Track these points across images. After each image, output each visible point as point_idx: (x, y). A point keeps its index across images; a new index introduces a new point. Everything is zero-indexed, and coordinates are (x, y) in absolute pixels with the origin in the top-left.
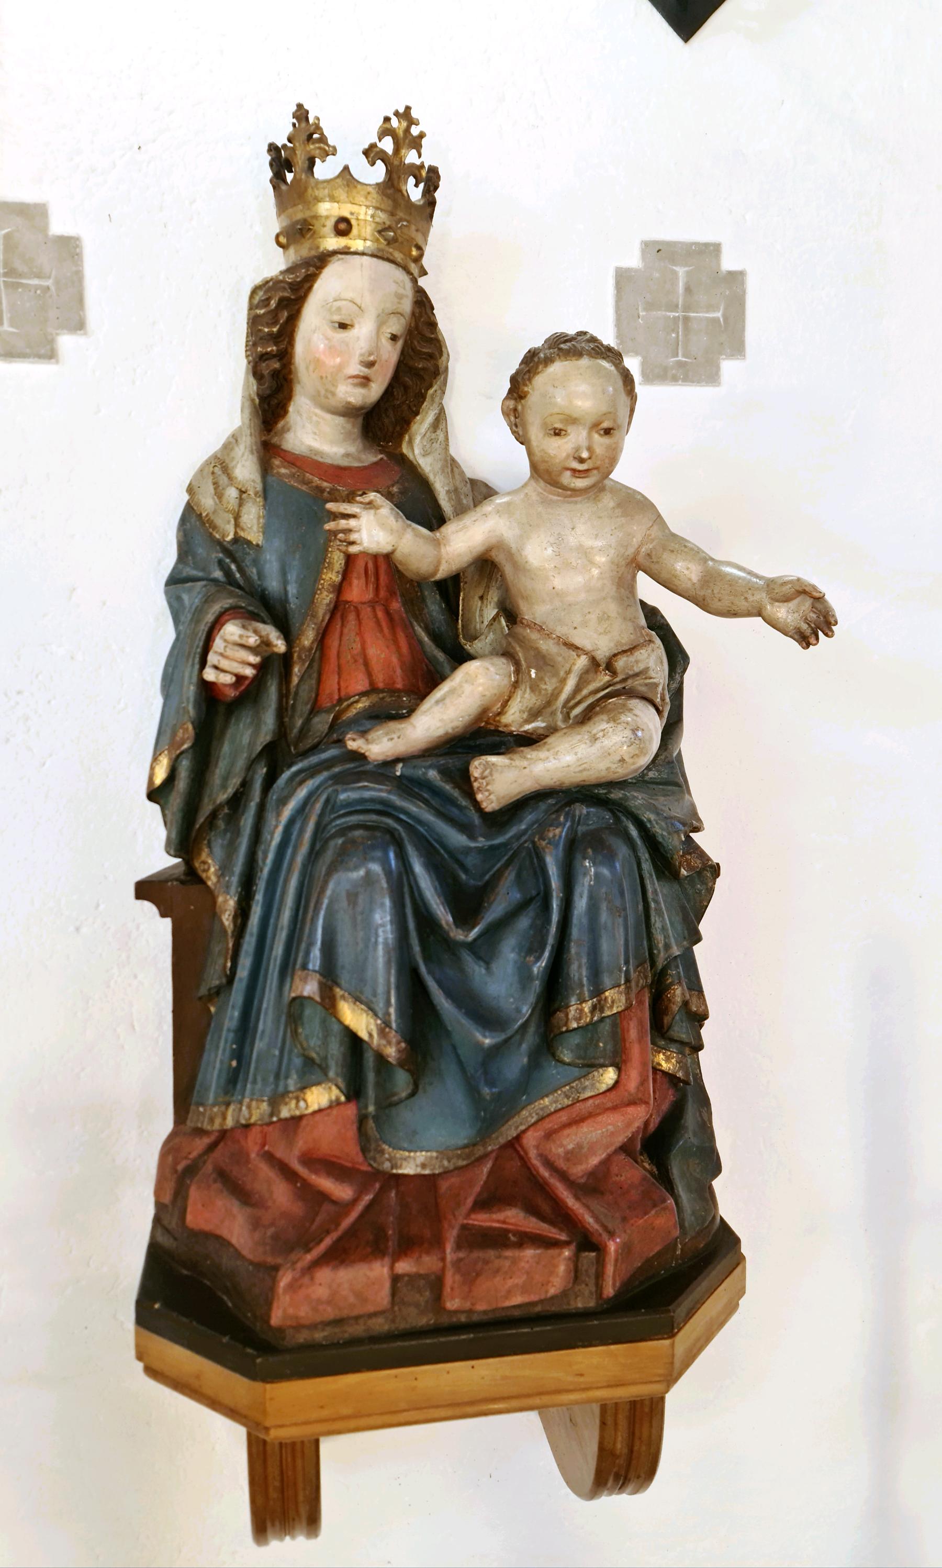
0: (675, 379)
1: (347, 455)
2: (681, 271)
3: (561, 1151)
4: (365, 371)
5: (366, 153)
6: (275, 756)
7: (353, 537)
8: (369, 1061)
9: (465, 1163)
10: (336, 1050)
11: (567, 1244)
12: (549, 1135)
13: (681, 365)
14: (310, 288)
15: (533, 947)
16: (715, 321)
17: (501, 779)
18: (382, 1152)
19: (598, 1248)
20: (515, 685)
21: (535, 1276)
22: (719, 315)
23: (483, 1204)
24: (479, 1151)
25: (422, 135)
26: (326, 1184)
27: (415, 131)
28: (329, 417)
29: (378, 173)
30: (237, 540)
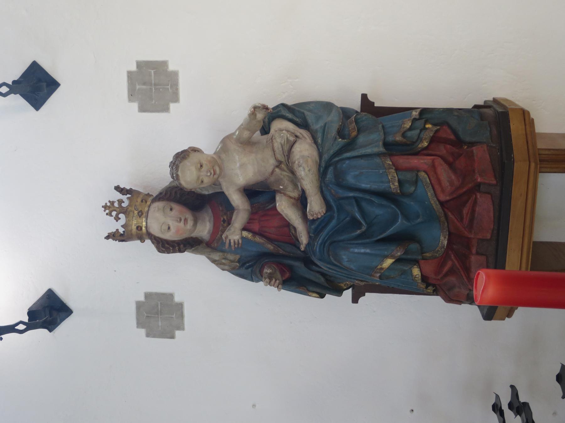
0: (177, 89)
1: (210, 221)
2: (138, 87)
3: (449, 187)
4: (183, 221)
5: (117, 221)
6: (308, 262)
7: (236, 241)
8: (404, 257)
9: (446, 224)
10: (400, 266)
11: (476, 195)
12: (443, 191)
13: (171, 87)
14: (158, 237)
15: (371, 202)
16: (155, 73)
17: (316, 206)
18: (438, 251)
19: (479, 185)
20: (285, 194)
21: (485, 206)
22: (152, 71)
23: (462, 219)
24: (443, 219)
25: (110, 202)
26: (446, 269)
27: (109, 204)
28: (197, 228)
29: (121, 216)
30: (239, 261)
